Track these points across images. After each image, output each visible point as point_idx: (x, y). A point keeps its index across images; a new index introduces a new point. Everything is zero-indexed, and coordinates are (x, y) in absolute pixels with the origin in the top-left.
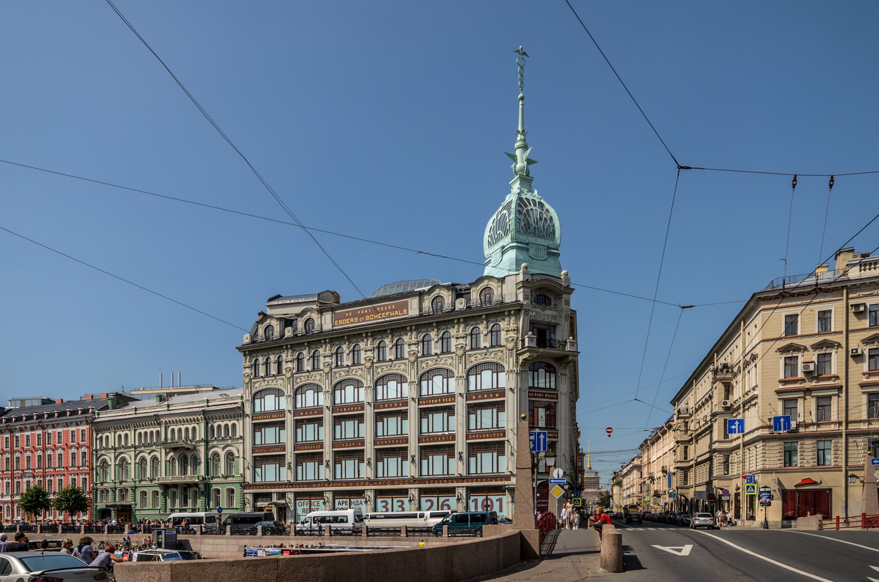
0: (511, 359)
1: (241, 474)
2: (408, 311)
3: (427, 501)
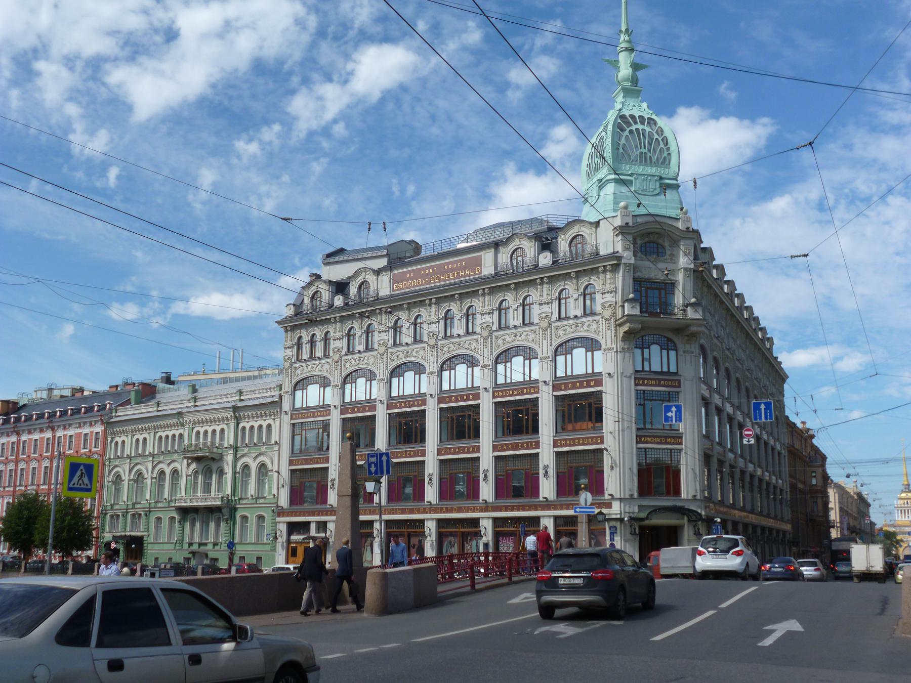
0: (609, 332)
1: (274, 495)
2: (481, 269)
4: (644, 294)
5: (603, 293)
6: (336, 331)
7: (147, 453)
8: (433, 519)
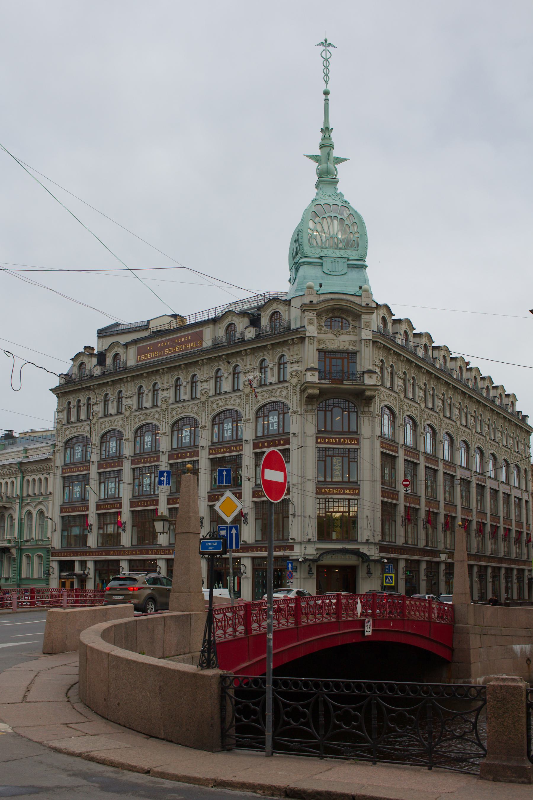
0: (295, 397)
1: (49, 538)
2: (202, 342)
6: (96, 397)
7: (14, 496)
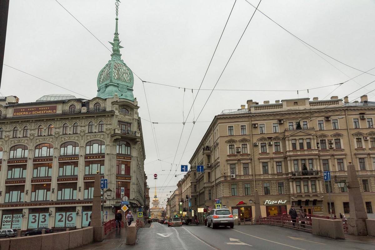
0: (108, 139)
2: (56, 111)
3: (59, 215)
4: (121, 126)
5: (107, 125)
8: (27, 208)
